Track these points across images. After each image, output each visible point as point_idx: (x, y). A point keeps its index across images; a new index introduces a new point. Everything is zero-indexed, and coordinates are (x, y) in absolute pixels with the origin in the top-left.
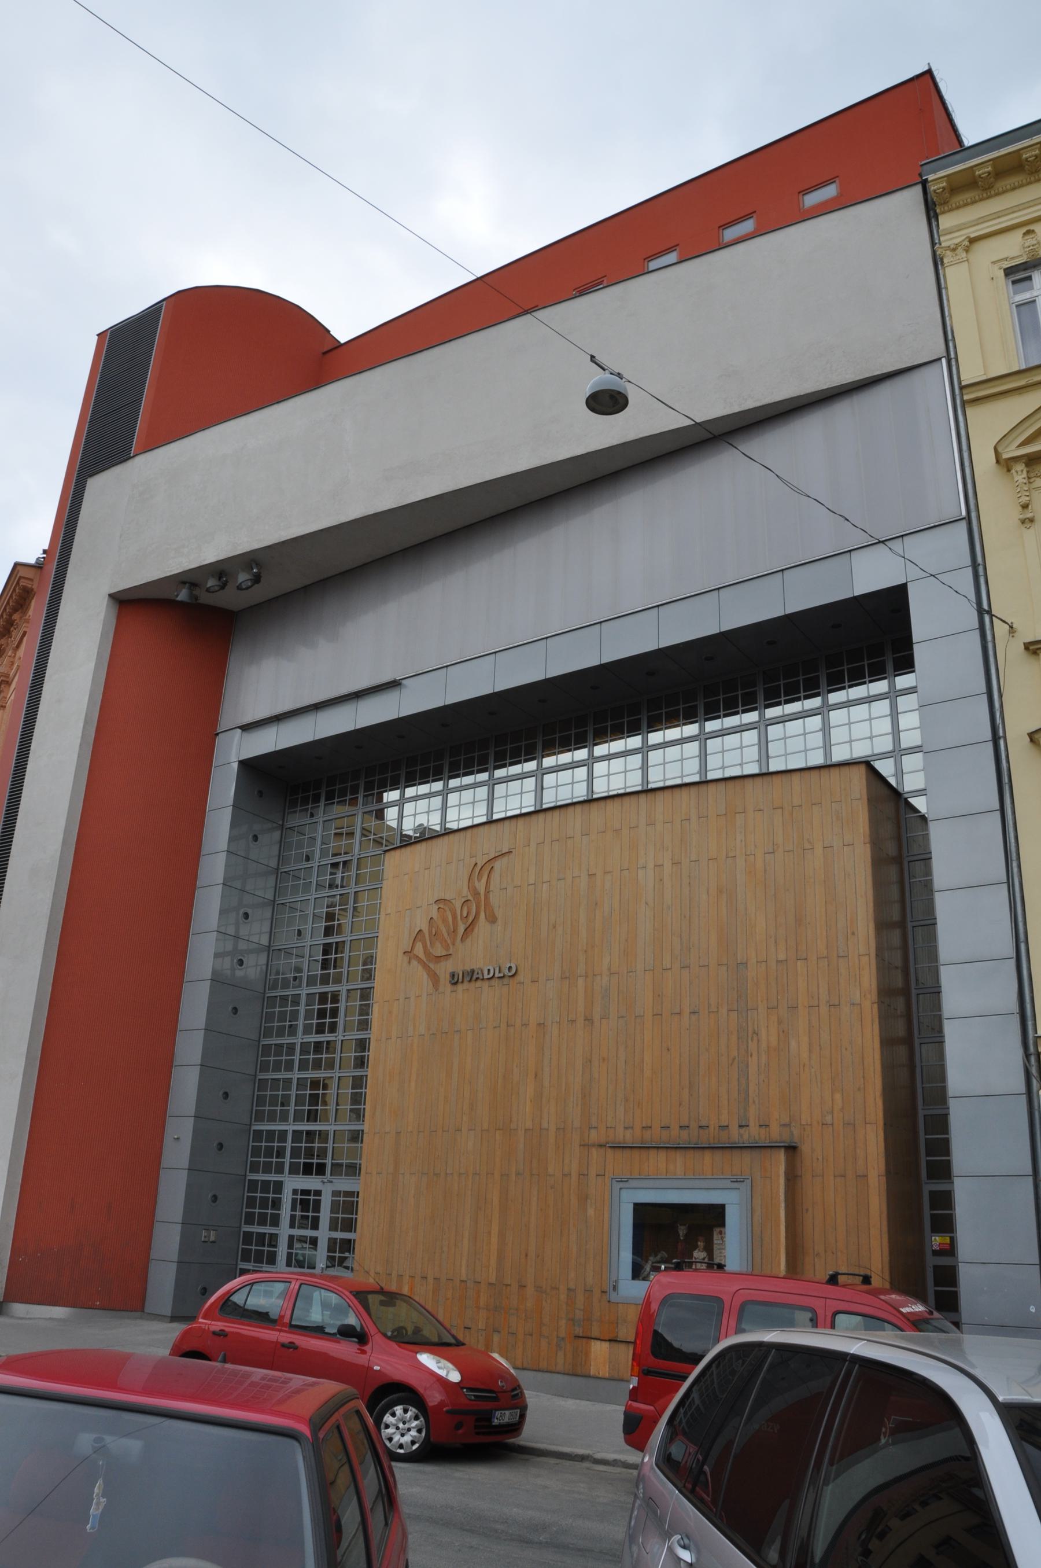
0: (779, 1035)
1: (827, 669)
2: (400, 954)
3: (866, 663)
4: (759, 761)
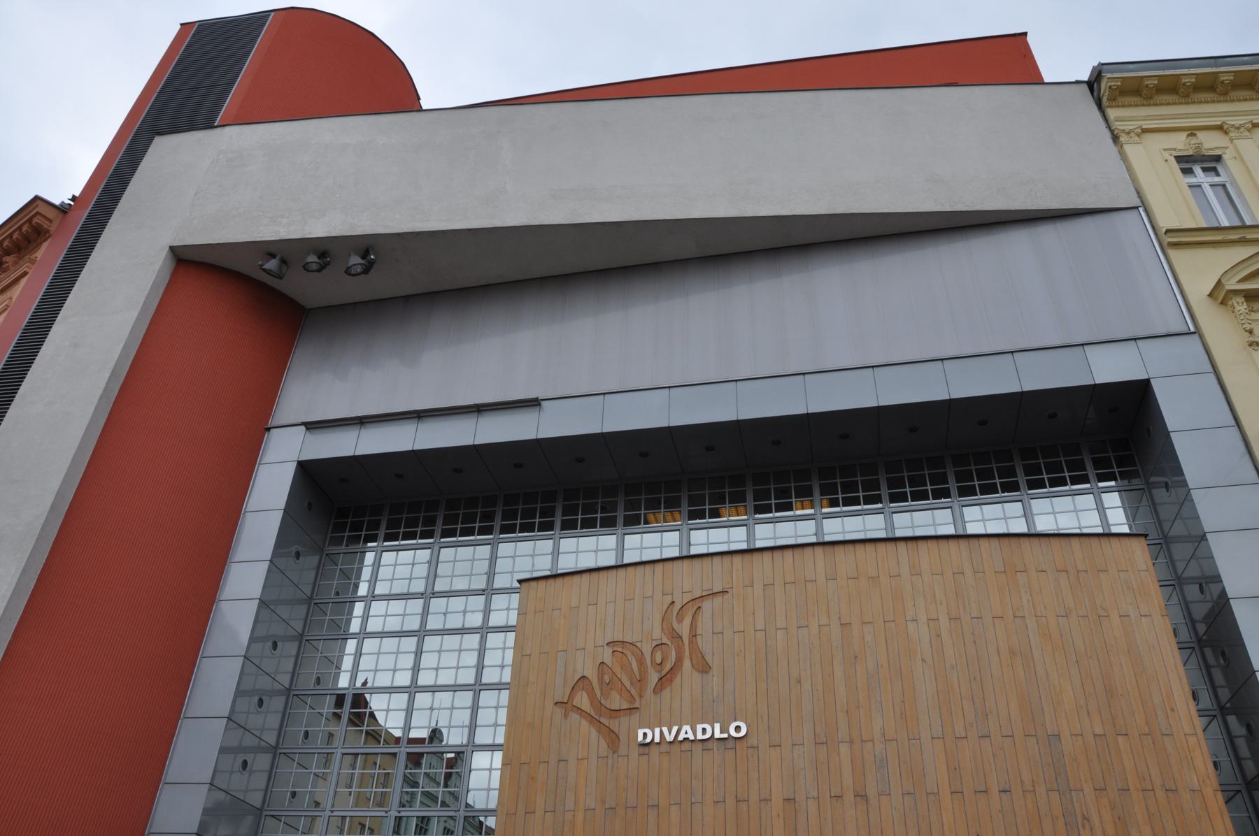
0: (1115, 823)
1: (627, 495)
2: (549, 705)
3: (581, 502)
4: (680, 546)
